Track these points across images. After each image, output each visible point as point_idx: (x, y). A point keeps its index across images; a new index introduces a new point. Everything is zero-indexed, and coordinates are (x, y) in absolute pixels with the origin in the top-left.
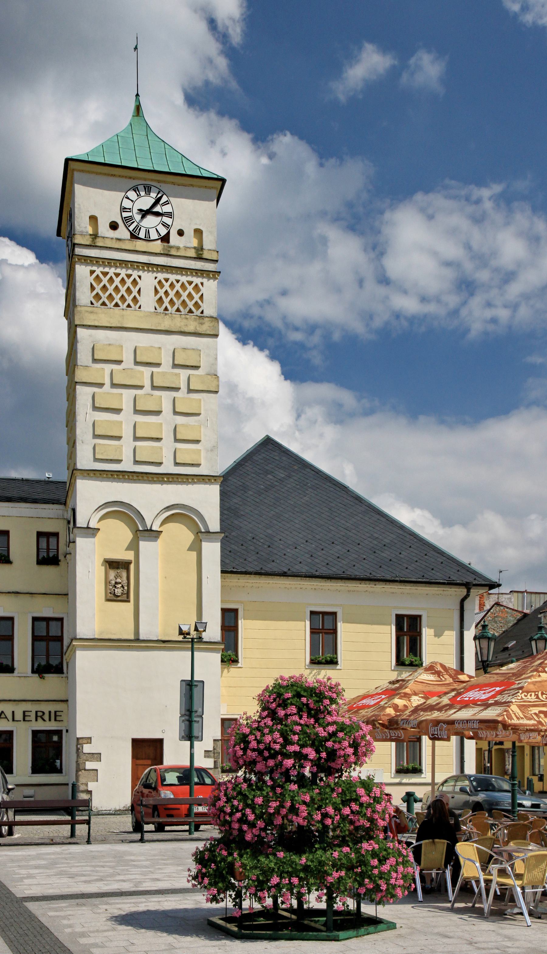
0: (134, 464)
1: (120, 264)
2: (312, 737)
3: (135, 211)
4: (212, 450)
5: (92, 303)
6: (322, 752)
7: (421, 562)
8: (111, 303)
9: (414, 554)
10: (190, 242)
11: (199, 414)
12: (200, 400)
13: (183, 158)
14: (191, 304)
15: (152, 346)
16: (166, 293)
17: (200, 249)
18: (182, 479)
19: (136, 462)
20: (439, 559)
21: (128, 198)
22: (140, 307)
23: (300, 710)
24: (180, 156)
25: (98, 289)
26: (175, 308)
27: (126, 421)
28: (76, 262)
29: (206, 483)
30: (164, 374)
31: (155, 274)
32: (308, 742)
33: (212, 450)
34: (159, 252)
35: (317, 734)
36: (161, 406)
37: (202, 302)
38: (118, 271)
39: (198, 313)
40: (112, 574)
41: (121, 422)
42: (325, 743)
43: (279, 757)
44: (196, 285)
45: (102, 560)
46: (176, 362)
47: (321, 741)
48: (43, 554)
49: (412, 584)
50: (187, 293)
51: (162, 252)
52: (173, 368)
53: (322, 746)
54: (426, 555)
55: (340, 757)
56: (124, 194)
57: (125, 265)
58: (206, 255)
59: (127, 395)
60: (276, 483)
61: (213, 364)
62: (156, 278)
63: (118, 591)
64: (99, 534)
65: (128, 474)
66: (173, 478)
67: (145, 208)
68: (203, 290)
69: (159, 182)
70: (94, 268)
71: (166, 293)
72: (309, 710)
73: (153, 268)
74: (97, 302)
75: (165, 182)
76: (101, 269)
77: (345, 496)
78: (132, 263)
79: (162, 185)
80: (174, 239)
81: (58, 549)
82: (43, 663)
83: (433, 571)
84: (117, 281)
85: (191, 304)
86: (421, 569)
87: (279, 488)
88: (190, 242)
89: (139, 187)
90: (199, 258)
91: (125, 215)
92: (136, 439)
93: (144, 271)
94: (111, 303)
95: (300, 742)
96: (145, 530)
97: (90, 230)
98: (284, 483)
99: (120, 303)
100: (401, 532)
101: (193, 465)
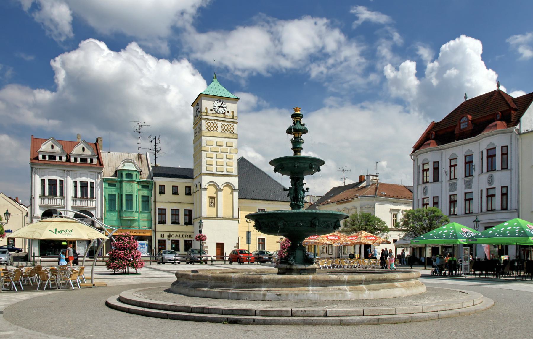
14: (231, 130)
17: (233, 116)
27: (214, 160)
40: (211, 200)
59: (215, 154)
80: (227, 114)
85: (231, 130)
90: (233, 118)
92: (217, 165)
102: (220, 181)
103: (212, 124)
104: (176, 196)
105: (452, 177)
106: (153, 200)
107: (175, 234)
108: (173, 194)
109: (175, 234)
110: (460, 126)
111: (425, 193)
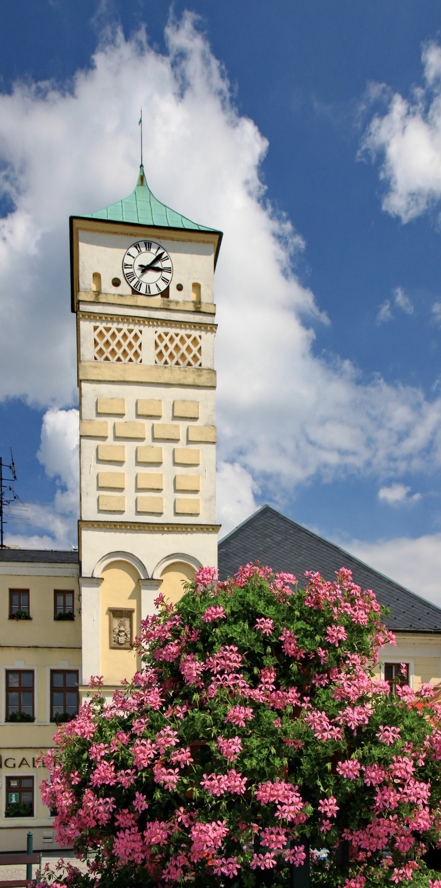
0: (136, 515)
1: (122, 319)
2: (292, 745)
3: (136, 267)
4: (210, 500)
5: (95, 359)
6: (325, 796)
7: (409, 613)
8: (113, 357)
9: (401, 606)
10: (189, 296)
11: (197, 465)
12: (199, 451)
13: (184, 219)
14: (189, 357)
15: (152, 399)
16: (166, 347)
17: (198, 303)
18: (182, 528)
19: (138, 513)
20: (425, 611)
21: (130, 255)
22: (141, 362)
23: (252, 660)
24: (180, 217)
25: (101, 345)
26: (175, 361)
27: (128, 473)
28: (80, 318)
29: (204, 532)
30: (164, 426)
31: (155, 329)
32: (277, 762)
33: (210, 500)
34: (159, 306)
35: (308, 739)
36: (162, 458)
37: (200, 354)
38: (120, 326)
39: (197, 365)
40: (116, 622)
41: (123, 474)
42: (334, 766)
43: (181, 814)
44: (195, 339)
45: (106, 609)
46: (175, 414)
47: (319, 761)
48: (60, 610)
49: (400, 634)
50: (186, 346)
51: (162, 307)
52: (172, 420)
53: (323, 774)
54: (413, 606)
55: (384, 813)
56: (126, 250)
57: (127, 320)
58: (203, 309)
59: (130, 447)
60: (274, 545)
61: (211, 416)
62: (156, 332)
63: (122, 640)
64: (104, 584)
65: (131, 524)
66: (173, 528)
67: (145, 264)
68: (201, 343)
69: (159, 238)
70: (98, 324)
71: (166, 347)
72: (283, 662)
73: (153, 323)
74: (101, 357)
75: (164, 238)
76: (104, 325)
77: (336, 555)
78: (133, 318)
79: (162, 241)
80: (174, 293)
81: (73, 606)
82: (61, 712)
83: (420, 621)
84: (119, 336)
85: (189, 357)
86: (408, 619)
87: (276, 550)
88: (189, 296)
89: (140, 244)
90: (198, 311)
91: (127, 271)
92: (138, 490)
93: (145, 325)
94: (113, 357)
95: (247, 762)
96: (147, 579)
97: (94, 288)
98: (281, 545)
99: (122, 358)
100: (389, 587)
101: (191, 515)
103: (119, 336)
104: (21, 626)
107: (18, 756)
108: (12, 617)
109: (18, 756)
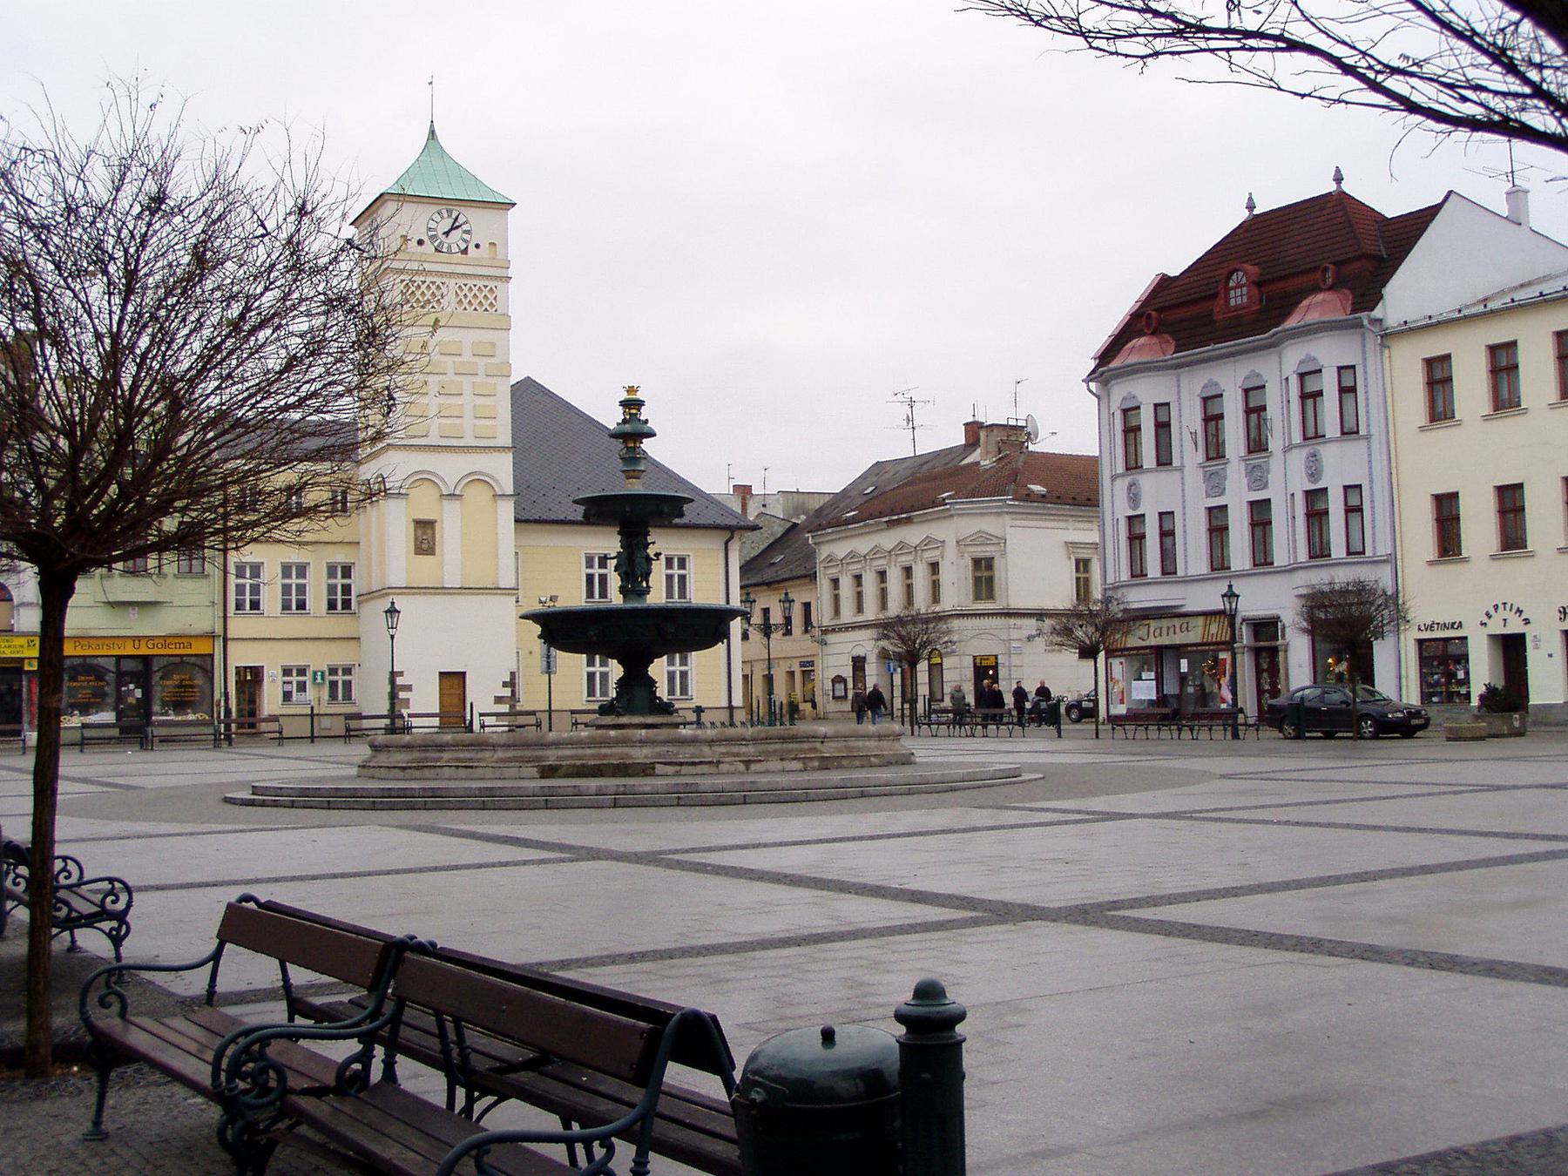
102: (451, 469)
105: (1311, 433)
106: (1453, 757)
110: (1227, 299)
111: (1134, 499)
